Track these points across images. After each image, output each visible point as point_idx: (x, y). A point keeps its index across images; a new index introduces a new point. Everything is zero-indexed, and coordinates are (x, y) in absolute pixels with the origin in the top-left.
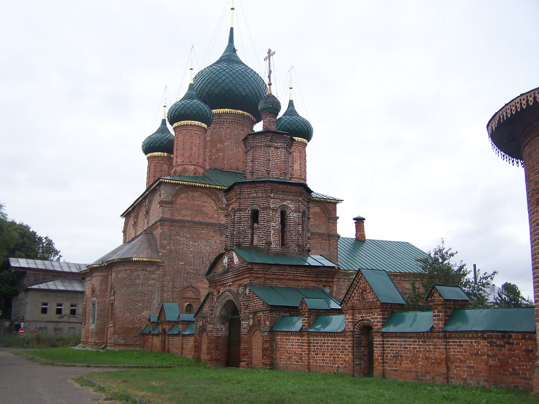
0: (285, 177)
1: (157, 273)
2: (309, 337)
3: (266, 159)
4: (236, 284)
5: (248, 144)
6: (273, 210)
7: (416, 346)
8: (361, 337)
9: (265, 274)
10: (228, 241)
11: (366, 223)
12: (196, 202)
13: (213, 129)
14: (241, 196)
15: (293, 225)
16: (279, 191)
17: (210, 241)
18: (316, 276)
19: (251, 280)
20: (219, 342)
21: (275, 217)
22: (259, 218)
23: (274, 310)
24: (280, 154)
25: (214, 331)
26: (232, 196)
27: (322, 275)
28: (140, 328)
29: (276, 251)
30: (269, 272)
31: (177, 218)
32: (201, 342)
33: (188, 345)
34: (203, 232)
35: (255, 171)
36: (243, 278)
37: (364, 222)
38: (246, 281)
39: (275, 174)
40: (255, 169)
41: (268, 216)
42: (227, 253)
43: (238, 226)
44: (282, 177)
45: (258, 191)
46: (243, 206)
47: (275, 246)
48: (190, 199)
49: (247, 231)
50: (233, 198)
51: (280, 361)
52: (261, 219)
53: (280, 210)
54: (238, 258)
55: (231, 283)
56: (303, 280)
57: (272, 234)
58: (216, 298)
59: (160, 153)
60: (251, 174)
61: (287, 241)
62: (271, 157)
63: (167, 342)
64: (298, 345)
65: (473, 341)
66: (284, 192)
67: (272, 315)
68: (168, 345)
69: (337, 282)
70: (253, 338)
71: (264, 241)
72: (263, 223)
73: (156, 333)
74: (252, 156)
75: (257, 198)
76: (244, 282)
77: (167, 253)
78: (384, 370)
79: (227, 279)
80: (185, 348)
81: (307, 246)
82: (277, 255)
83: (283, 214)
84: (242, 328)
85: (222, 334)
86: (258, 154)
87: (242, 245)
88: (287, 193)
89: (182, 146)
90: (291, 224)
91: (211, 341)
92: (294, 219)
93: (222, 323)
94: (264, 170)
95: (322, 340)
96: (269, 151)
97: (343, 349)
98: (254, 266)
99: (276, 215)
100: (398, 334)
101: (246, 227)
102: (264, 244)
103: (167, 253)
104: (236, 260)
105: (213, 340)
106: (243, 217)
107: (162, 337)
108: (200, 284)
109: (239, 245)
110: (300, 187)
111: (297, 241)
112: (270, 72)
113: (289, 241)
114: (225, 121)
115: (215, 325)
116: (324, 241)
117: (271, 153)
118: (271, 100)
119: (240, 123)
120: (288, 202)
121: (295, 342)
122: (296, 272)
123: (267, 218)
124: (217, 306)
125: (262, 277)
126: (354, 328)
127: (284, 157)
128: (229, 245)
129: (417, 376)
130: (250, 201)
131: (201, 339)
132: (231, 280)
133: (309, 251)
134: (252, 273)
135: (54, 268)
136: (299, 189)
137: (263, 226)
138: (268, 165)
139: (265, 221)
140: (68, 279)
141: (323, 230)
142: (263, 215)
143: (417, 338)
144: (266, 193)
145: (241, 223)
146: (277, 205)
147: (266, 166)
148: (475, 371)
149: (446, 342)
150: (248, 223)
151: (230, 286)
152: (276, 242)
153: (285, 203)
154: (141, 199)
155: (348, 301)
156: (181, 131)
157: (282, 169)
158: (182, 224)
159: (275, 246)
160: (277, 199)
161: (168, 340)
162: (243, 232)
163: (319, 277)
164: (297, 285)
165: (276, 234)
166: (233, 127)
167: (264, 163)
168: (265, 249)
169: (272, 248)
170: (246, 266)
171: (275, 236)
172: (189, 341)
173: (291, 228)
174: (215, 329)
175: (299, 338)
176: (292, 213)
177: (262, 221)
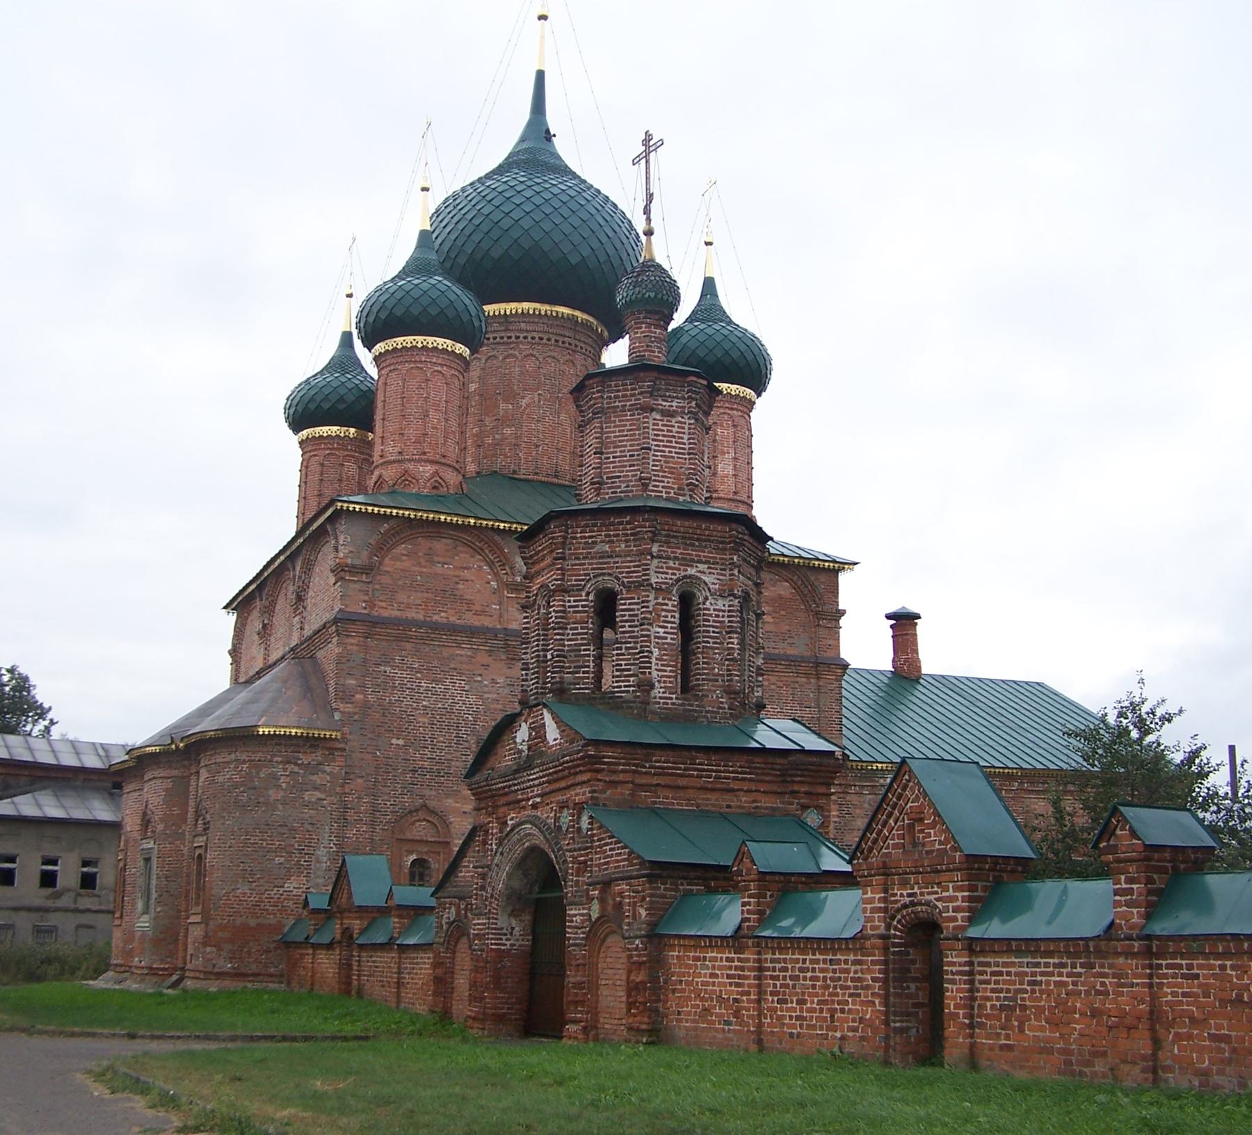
0: (691, 496)
1: (328, 769)
2: (759, 953)
7: (1065, 979)
8: (908, 954)
9: (634, 772)
11: (921, 628)
12: (438, 569)
13: (487, 360)
14: (567, 552)
15: (714, 632)
17: (479, 678)
18: (780, 779)
19: (594, 791)
20: (504, 967)
21: (663, 610)
23: (659, 876)
24: (677, 432)
25: (491, 936)
27: (796, 776)
28: (280, 926)
30: (645, 767)
31: (385, 614)
32: (453, 968)
34: (458, 652)
35: (608, 478)
36: (573, 785)
37: (916, 624)
38: (581, 794)
39: (663, 487)
40: (605, 473)
41: (642, 607)
42: (526, 712)
43: (558, 637)
45: (614, 536)
46: (571, 580)
47: (664, 693)
48: (422, 560)
49: (584, 650)
51: (679, 1021)
52: (624, 616)
53: (677, 590)
54: (558, 727)
55: (538, 800)
56: (742, 790)
57: (653, 660)
58: (494, 842)
59: (335, 428)
60: (596, 489)
61: (698, 680)
62: (653, 440)
63: (355, 968)
64: (729, 976)
65: (1228, 963)
66: (688, 540)
67: (655, 888)
68: (359, 976)
69: (841, 795)
71: (632, 679)
72: (630, 626)
73: (326, 939)
74: (597, 438)
75: (611, 557)
76: (576, 795)
77: (355, 714)
78: (972, 1046)
79: (528, 788)
81: (756, 694)
82: (669, 718)
83: (687, 603)
85: (511, 945)
86: (615, 432)
87: (570, 689)
90: (709, 632)
91: (482, 964)
92: (717, 616)
93: (513, 914)
94: (633, 476)
95: (797, 961)
97: (856, 988)
98: (605, 749)
99: (667, 605)
100: (1014, 943)
101: (582, 639)
102: (632, 689)
103: (355, 714)
104: (552, 733)
105: (487, 962)
106: (572, 610)
107: (341, 952)
108: (449, 801)
109: (561, 692)
110: (734, 526)
111: (726, 678)
112: (650, 197)
113: (703, 679)
114: (522, 336)
115: (493, 918)
116: (804, 680)
117: (651, 427)
119: (563, 342)
120: (702, 567)
121: (720, 968)
122: (722, 769)
124: (497, 865)
125: (627, 782)
126: (888, 927)
127: (689, 439)
128: (531, 690)
129: (1068, 1063)
130: (592, 564)
132: (537, 791)
133: (760, 706)
134: (598, 771)
135: (33, 756)
137: (629, 637)
139: (636, 623)
140: (75, 788)
141: (799, 648)
142: (630, 604)
143: (1069, 954)
144: (637, 543)
145: (566, 629)
146: (670, 577)
147: (638, 465)
148: (1234, 1050)
149: (1150, 966)
151: (535, 806)
152: (665, 682)
153: (691, 571)
154: (282, 558)
155: (871, 849)
158: (400, 629)
159: (663, 692)
160: (669, 558)
161: (359, 961)
162: (572, 654)
163: (788, 782)
164: (725, 804)
165: (665, 660)
167: (633, 455)
168: (634, 702)
169: (655, 698)
170: (579, 752)
171: (662, 665)
173: (709, 643)
175: (733, 955)
176: (711, 600)
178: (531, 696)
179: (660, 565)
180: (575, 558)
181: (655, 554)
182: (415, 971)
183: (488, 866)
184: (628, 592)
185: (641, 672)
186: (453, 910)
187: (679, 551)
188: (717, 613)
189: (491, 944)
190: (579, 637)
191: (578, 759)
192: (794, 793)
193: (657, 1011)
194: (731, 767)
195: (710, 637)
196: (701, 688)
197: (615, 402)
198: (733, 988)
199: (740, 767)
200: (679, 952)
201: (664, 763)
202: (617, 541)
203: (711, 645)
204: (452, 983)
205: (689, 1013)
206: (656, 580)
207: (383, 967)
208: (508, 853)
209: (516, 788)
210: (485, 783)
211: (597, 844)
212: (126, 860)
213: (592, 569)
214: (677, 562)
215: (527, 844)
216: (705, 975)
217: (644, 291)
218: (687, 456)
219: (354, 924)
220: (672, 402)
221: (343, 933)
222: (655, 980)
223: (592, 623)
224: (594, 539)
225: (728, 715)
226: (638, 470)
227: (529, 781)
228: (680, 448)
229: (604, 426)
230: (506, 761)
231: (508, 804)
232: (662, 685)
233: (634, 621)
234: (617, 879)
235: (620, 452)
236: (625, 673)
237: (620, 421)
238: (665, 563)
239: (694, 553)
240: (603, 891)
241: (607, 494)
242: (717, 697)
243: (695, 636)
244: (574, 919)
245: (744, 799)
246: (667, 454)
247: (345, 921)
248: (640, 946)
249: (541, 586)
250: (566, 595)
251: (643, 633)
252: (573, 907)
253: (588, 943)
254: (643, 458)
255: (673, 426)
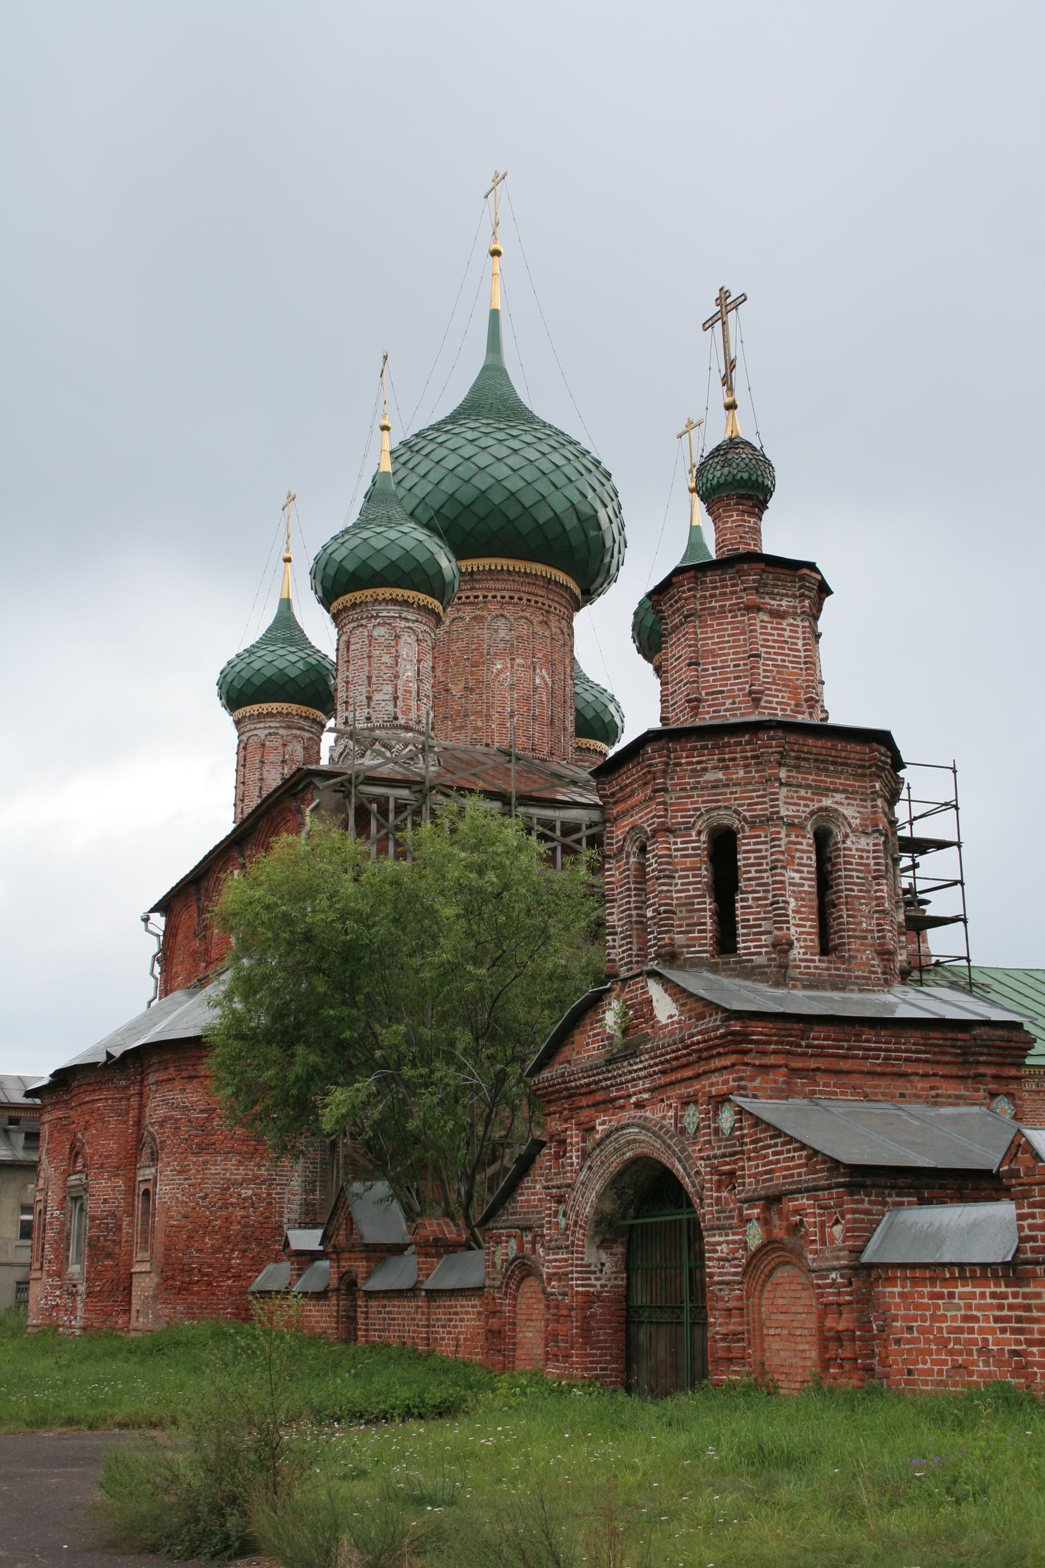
3: (745, 652)
4: (668, 1098)
5: (671, 606)
6: (790, 825)
9: (788, 1053)
10: (616, 944)
14: (669, 782)
15: (858, 878)
16: (805, 759)
18: (961, 1059)
19: (741, 1079)
20: (593, 1315)
21: (797, 850)
22: (739, 857)
23: (863, 1186)
24: (790, 637)
25: (575, 1275)
26: (631, 783)
27: (981, 1054)
29: (807, 974)
30: (800, 1046)
32: (514, 1318)
33: (455, 1327)
35: (707, 694)
36: (705, 1073)
39: (777, 703)
40: (704, 688)
41: (772, 847)
43: (665, 888)
44: (803, 713)
45: (731, 760)
46: (676, 817)
47: (805, 954)
49: (699, 903)
50: (633, 791)
52: (749, 858)
53: (812, 825)
54: (676, 1001)
55: (646, 1096)
56: (916, 1074)
57: (790, 912)
58: (575, 1154)
61: (841, 937)
62: (762, 646)
63: (361, 1321)
64: (997, 1319)
66: (822, 763)
67: (857, 1202)
70: (766, 1295)
71: (763, 937)
72: (757, 871)
74: (690, 646)
75: (728, 786)
76: (712, 1085)
79: (628, 1082)
80: (443, 1339)
81: (900, 958)
83: (823, 840)
84: (710, 1259)
85: (602, 1286)
86: (713, 638)
87: (682, 953)
88: (832, 768)
89: (367, 668)
90: (852, 877)
91: (565, 1312)
93: (604, 1245)
94: (740, 690)
95: (972, 1296)
96: (754, 625)
98: (753, 1023)
99: (801, 844)
101: (695, 890)
102: (764, 950)
105: (572, 1309)
106: (679, 853)
107: (338, 1300)
110: (875, 746)
111: (876, 935)
112: (731, 365)
113: (849, 937)
114: (490, 595)
115: (577, 1252)
117: (759, 631)
118: (744, 456)
119: (536, 602)
120: (839, 797)
121: (979, 1308)
122: (893, 1046)
123: (772, 854)
124: (583, 1184)
125: (779, 1066)
127: (804, 645)
128: (622, 959)
130: (703, 796)
131: (515, 1306)
134: (745, 1052)
136: (872, 751)
138: (752, 674)
139: (765, 867)
142: (755, 844)
144: (760, 767)
145: (674, 878)
146: (804, 811)
147: (745, 676)
150: (700, 876)
152: (805, 940)
153: (827, 802)
156: (364, 622)
157: (801, 687)
160: (800, 786)
161: (367, 1313)
162: (684, 909)
163: (972, 1063)
165: (804, 913)
166: (517, 615)
167: (739, 665)
168: (769, 966)
169: (795, 960)
171: (800, 919)
172: (456, 1313)
173: (852, 890)
174: (577, 1266)
175: (1003, 1289)
177: (752, 865)
178: (621, 966)
179: (790, 794)
180: (681, 790)
181: (783, 781)
182: (453, 1323)
183: (569, 1186)
184: (752, 828)
185: (777, 928)
186: (513, 1243)
187: (811, 777)
188: (860, 853)
189: (577, 1286)
190: (691, 887)
191: (716, 1038)
192: (979, 1077)
193: (869, 1369)
194: (904, 1044)
195: (854, 884)
196: (847, 947)
197: (710, 602)
198: (1008, 1335)
199: (914, 1044)
200: (903, 1287)
201: (824, 1040)
202: (734, 766)
203: (856, 893)
204: (514, 1337)
205: (930, 1372)
206: (787, 813)
207: (403, 1319)
208: (599, 1166)
209: (608, 1083)
210: (560, 1080)
211: (751, 1147)
212: (46, 1201)
213: (703, 802)
214: (809, 791)
215: (628, 1155)
216: (954, 1318)
217: (735, 471)
218: (802, 666)
219: (358, 1266)
220: (781, 600)
221: (340, 1279)
222: (866, 1326)
223: (706, 869)
224: (703, 765)
225: (882, 982)
226: (747, 682)
227: (630, 1072)
228: (795, 656)
229: (699, 631)
230: (589, 1050)
231: (595, 1105)
232: (802, 944)
233: (761, 864)
234: (792, 1192)
235: (721, 661)
236: (755, 930)
237: (718, 624)
238: (796, 792)
239: (829, 780)
240: (767, 1209)
241: (708, 713)
242: (867, 958)
243: (834, 883)
244: (719, 1248)
245: (919, 1085)
246: (779, 663)
247: (343, 1264)
248: (839, 1280)
249: (632, 828)
250: (671, 836)
251: (777, 878)
252: (717, 1232)
253: (745, 1280)
254: (752, 668)
255: (785, 630)
